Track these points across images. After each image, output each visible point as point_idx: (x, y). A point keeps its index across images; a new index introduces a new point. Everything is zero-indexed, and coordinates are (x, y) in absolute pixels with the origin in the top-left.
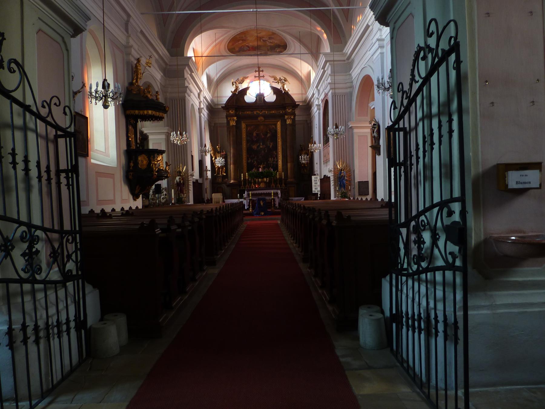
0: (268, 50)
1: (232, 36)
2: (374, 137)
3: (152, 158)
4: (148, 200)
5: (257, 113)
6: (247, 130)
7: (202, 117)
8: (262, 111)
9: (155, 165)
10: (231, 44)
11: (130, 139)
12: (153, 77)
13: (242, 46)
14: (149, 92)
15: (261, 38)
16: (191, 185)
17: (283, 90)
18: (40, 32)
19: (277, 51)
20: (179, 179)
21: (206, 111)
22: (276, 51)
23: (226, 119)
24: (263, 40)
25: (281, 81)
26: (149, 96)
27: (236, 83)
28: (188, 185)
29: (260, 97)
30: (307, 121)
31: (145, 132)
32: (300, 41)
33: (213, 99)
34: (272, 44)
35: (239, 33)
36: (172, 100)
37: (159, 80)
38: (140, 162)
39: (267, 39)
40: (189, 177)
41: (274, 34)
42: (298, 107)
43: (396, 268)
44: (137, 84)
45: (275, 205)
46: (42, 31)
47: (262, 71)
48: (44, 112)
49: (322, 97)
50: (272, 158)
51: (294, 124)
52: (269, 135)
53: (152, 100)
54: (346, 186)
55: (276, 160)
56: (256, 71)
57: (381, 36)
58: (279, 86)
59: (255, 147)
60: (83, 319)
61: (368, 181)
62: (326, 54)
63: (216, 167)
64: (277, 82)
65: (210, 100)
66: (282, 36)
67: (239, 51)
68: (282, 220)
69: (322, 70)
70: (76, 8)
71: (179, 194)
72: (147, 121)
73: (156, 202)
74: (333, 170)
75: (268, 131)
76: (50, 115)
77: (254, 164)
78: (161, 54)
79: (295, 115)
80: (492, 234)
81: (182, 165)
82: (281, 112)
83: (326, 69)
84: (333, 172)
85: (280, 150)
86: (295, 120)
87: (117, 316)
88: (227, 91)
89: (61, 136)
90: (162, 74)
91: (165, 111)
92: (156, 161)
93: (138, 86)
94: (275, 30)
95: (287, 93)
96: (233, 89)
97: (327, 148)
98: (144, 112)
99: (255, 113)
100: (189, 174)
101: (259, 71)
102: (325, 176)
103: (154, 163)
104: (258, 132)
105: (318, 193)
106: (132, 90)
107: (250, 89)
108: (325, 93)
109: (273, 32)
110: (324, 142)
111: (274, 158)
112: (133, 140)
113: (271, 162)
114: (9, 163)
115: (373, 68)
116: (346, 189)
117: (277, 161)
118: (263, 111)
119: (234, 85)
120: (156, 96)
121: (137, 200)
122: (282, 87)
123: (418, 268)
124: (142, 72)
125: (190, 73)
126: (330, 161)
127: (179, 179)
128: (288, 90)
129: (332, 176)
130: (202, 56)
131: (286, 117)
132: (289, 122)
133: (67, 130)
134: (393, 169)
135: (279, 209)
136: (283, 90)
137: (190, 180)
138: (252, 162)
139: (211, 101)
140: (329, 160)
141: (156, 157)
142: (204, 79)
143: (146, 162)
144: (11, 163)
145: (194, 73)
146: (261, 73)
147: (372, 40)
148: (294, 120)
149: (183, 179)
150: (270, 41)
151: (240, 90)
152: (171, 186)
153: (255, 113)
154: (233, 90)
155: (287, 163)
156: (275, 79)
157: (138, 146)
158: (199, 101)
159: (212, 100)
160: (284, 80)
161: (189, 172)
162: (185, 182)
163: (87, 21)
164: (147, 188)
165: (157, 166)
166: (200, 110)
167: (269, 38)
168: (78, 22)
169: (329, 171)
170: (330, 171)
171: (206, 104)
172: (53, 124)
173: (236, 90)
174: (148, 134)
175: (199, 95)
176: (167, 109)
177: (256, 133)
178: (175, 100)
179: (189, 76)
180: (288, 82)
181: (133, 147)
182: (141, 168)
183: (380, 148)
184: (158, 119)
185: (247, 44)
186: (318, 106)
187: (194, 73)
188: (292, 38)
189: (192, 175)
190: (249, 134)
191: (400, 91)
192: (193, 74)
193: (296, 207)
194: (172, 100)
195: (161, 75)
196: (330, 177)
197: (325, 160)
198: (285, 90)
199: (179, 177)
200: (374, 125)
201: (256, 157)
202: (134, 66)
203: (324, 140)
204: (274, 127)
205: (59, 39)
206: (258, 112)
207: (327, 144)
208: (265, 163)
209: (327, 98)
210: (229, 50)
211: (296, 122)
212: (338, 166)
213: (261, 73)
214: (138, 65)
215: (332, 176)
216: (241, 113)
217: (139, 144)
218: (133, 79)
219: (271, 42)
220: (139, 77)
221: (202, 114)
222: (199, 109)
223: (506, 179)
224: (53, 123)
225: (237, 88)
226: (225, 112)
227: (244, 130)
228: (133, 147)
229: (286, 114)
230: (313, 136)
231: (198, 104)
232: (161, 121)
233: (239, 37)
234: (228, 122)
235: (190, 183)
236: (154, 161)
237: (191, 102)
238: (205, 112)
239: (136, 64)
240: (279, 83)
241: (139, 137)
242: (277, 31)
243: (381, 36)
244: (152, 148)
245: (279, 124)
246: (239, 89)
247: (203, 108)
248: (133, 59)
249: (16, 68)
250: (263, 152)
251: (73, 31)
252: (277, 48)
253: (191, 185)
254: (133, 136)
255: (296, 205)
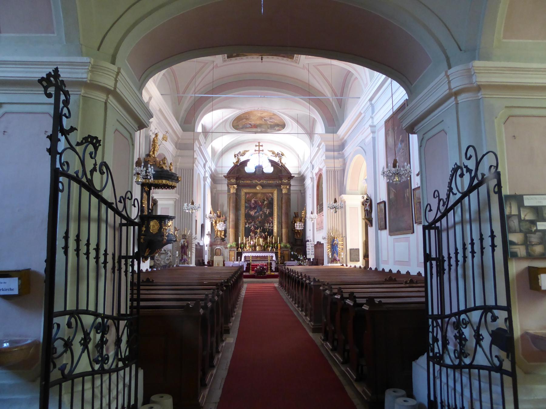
0: (268, 128)
1: (238, 115)
2: (367, 210)
3: (163, 223)
4: (153, 261)
5: (256, 182)
6: (245, 197)
7: (206, 185)
8: (260, 180)
9: (166, 229)
10: (235, 122)
11: (144, 205)
12: (166, 149)
13: (246, 124)
14: (165, 163)
15: (262, 118)
16: (194, 248)
17: (280, 163)
18: (117, 132)
19: (276, 129)
20: (183, 242)
21: (210, 180)
22: (275, 129)
23: (227, 187)
24: (264, 120)
25: (279, 155)
26: (164, 167)
27: (237, 155)
28: (192, 247)
29: (259, 168)
30: (301, 191)
31: (154, 198)
32: (298, 122)
33: (217, 168)
34: (272, 124)
35: (244, 112)
36: (181, 170)
37: (171, 152)
38: (151, 227)
39: (267, 119)
40: (193, 240)
41: (274, 115)
42: (294, 178)
43: (438, 360)
44: (153, 156)
45: (271, 267)
46: (118, 131)
47: (262, 146)
48: (120, 207)
49: (316, 170)
50: (268, 224)
51: (288, 194)
52: (266, 202)
53: (167, 171)
54: (338, 253)
55: (271, 225)
56: (256, 146)
57: (373, 122)
58: (276, 159)
59: (252, 213)
60: (133, 403)
61: (359, 249)
62: (320, 135)
63: (216, 230)
64: (274, 156)
65: (214, 170)
66: (282, 117)
67: (242, 128)
68: (281, 283)
69: (318, 148)
70: (144, 109)
71: (182, 256)
72: (160, 189)
73: (161, 263)
74: (326, 237)
75: (266, 199)
76: (124, 209)
77: (251, 228)
78: (175, 129)
79: (290, 186)
80: (528, 330)
81: (187, 229)
82: (278, 182)
83: (321, 147)
84: (326, 240)
85: (275, 217)
86: (290, 190)
87: (162, 397)
88: (229, 163)
89: (124, 225)
90: (174, 147)
91: (177, 180)
92: (167, 227)
93: (154, 157)
94: (276, 112)
95: (283, 167)
96: (235, 160)
97: (321, 216)
98: (159, 181)
99: (254, 182)
100: (193, 238)
101: (259, 146)
102: (318, 242)
103: (165, 228)
104: (255, 200)
105: (136, 166)
106: (149, 160)
107: (250, 160)
108: (319, 168)
109: (274, 113)
110: (317, 211)
111: (270, 224)
112: (146, 206)
113: (268, 227)
114: (84, 253)
115: (366, 150)
116: (338, 255)
117: (273, 226)
118: (261, 181)
119: (236, 157)
120: (170, 167)
121: (146, 262)
122: (279, 161)
123: (460, 363)
124: (159, 144)
125: (198, 146)
126: (324, 228)
127: (184, 241)
128: (285, 163)
129: (325, 243)
130: (212, 132)
131: (282, 186)
132: (284, 191)
133: (135, 221)
134: (428, 264)
135: (275, 272)
136: (280, 163)
137: (194, 243)
138: (250, 227)
139: (214, 171)
140: (323, 228)
141: (167, 223)
142: (209, 150)
143: (157, 227)
144: (85, 254)
145: (202, 146)
146: (261, 147)
147: (364, 125)
148: (289, 190)
149: (187, 242)
150: (270, 121)
151: (241, 162)
152: (175, 248)
153: (254, 182)
154: (235, 162)
155: (282, 228)
156: (273, 153)
157: (150, 211)
158: (205, 170)
159: (216, 170)
160: (281, 154)
161: (193, 236)
162: (189, 245)
163: (149, 118)
164: (157, 250)
165: (167, 231)
166: (205, 179)
167: (270, 118)
168: (144, 120)
169: (322, 238)
170: (324, 238)
171: (210, 173)
172: (125, 216)
173: (237, 162)
174: (157, 200)
175: (205, 165)
176: (180, 179)
177: (254, 200)
178: (184, 170)
179: (197, 148)
180: (285, 156)
181: (146, 213)
182: (152, 233)
183: (372, 220)
184: (170, 188)
185: (250, 123)
186: (312, 179)
187: (202, 146)
188: (290, 119)
189: (195, 238)
190: (248, 201)
191: (436, 197)
192: (201, 147)
193: (291, 272)
194: (181, 170)
195: (173, 147)
196: (323, 244)
197: (319, 227)
198: (282, 163)
199: (183, 240)
200: (367, 199)
201: (253, 222)
202: (152, 140)
203: (317, 209)
204: (271, 195)
205: (128, 136)
206: (257, 181)
207: (320, 213)
208: (262, 228)
209: (321, 173)
210: (233, 127)
211: (291, 191)
212: (332, 234)
213: (261, 147)
214: (155, 139)
215: (325, 243)
216: (241, 182)
217: (151, 210)
218: (150, 152)
219: (271, 121)
220: (156, 149)
221: (206, 182)
222: (204, 177)
223: (540, 281)
224: (126, 215)
225: (239, 160)
226: (227, 180)
227: (243, 197)
228: (146, 213)
229: (282, 184)
230: (306, 205)
231: (203, 174)
232: (173, 189)
233: (244, 116)
234: (229, 190)
235: (193, 246)
236: (165, 226)
237: (198, 172)
238: (209, 180)
239: (154, 138)
240: (276, 156)
241: (152, 204)
242: (278, 112)
243: (373, 122)
244: (160, 214)
245: (275, 193)
246: (240, 161)
247: (207, 177)
248: (151, 134)
249: (105, 170)
250: (260, 218)
251: (138, 127)
252: (276, 127)
253: (194, 248)
254: (146, 202)
255: (291, 270)
